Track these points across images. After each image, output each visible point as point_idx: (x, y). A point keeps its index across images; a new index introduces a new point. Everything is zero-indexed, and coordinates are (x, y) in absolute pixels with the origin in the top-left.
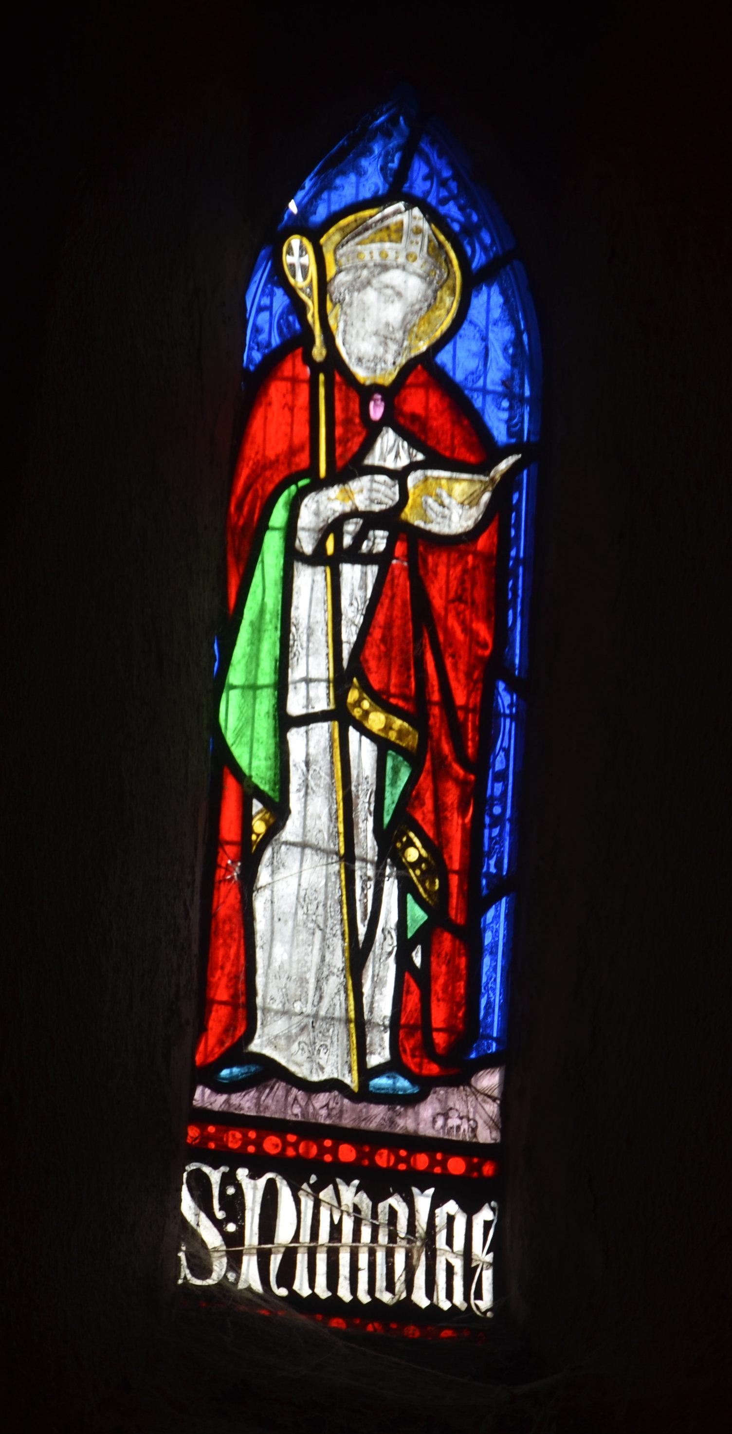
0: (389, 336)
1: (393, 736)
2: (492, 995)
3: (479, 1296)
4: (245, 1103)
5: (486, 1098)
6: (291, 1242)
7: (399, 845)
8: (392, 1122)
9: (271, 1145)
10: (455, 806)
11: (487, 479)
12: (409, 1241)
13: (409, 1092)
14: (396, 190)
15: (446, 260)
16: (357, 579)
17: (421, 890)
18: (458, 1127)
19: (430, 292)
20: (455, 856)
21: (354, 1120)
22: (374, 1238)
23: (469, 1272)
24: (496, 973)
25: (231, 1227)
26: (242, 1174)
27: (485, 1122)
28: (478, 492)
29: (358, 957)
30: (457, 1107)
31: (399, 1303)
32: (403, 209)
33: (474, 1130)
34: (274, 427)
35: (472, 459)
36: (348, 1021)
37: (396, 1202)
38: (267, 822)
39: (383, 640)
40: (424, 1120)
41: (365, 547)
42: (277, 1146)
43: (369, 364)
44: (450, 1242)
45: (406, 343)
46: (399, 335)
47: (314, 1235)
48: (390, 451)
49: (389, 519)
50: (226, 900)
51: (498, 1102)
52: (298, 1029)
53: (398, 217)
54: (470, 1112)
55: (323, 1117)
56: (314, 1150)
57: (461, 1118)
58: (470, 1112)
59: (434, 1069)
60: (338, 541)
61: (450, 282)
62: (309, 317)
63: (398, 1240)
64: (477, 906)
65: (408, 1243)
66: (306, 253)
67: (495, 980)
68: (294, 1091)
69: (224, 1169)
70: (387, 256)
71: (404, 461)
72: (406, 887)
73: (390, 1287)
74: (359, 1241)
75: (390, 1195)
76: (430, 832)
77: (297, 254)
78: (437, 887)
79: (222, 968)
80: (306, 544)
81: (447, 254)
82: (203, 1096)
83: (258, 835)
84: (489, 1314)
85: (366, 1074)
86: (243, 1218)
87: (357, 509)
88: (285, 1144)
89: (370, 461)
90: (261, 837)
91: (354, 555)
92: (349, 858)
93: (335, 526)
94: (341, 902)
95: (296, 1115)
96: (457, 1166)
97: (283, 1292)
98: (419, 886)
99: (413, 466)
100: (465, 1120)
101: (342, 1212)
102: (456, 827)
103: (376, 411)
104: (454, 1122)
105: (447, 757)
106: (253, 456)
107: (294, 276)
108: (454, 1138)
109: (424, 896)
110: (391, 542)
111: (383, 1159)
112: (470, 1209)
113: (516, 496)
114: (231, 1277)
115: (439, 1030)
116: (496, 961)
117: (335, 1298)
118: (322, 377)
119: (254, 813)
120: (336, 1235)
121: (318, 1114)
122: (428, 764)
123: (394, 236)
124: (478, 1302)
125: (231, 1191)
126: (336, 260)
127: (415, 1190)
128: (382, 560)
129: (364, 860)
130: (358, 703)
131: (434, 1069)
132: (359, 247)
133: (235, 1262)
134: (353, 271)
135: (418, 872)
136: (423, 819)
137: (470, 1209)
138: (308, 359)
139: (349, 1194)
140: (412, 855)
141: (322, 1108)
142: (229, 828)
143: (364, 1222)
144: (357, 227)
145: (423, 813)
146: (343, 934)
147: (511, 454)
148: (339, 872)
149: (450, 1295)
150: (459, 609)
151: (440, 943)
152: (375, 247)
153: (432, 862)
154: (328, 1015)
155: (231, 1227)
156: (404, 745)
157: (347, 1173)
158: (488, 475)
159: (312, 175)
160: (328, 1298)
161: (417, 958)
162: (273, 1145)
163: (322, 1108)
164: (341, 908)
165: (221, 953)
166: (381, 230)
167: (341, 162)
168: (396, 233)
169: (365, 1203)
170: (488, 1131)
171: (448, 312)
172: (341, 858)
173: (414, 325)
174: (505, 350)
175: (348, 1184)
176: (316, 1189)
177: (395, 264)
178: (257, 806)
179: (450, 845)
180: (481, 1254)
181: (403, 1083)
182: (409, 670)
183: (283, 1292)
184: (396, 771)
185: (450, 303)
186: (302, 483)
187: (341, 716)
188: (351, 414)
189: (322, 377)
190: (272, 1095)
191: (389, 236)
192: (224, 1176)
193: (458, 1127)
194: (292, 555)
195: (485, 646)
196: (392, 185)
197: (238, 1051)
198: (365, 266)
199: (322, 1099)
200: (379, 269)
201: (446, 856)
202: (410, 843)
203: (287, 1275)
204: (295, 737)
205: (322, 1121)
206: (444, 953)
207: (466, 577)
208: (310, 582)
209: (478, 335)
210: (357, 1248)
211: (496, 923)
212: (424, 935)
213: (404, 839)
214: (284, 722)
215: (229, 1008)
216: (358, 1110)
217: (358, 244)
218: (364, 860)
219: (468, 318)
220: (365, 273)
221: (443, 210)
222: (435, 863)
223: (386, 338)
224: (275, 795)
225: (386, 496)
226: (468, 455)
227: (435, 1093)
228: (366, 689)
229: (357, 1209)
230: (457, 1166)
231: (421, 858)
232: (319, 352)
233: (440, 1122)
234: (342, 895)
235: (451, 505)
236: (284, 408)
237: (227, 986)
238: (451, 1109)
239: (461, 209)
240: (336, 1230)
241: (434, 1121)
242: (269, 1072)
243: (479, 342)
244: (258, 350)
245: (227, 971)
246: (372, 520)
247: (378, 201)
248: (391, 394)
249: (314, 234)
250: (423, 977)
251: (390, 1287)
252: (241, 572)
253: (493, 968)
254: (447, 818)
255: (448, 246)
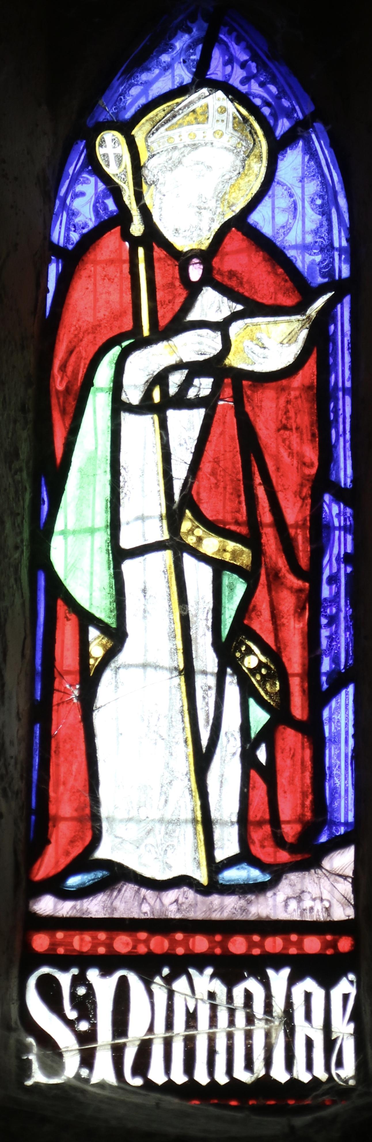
0: (203, 205)
1: (227, 557)
2: (337, 781)
3: (340, 1064)
4: (95, 907)
5: (337, 878)
6: (146, 1035)
7: (238, 655)
8: (244, 910)
9: (122, 944)
10: (292, 612)
11: (304, 317)
12: (267, 1021)
13: (260, 880)
14: (202, 79)
15: (250, 132)
16: (185, 424)
17: (262, 693)
18: (312, 908)
19: (239, 163)
20: (295, 660)
21: (205, 912)
22: (232, 1023)
23: (329, 1044)
24: (340, 760)
25: (84, 1026)
26: (93, 975)
27: (338, 901)
28: (296, 330)
29: (203, 760)
30: (310, 890)
31: (259, 1081)
32: (207, 94)
33: (327, 910)
34: (96, 298)
35: (289, 301)
36: (194, 821)
37: (252, 984)
38: (104, 646)
39: (214, 473)
40: (275, 906)
41: (192, 393)
42: (128, 944)
43: (185, 234)
44: (308, 1017)
45: (219, 210)
46: (212, 204)
47: (169, 1025)
48: (211, 305)
49: (214, 367)
50: (65, 721)
51: (350, 880)
52: (144, 833)
53: (203, 102)
54: (326, 892)
55: (173, 913)
56: (166, 944)
57: (314, 900)
58: (326, 892)
59: (284, 856)
60: (164, 392)
61: (256, 151)
62: (126, 199)
63: (256, 1021)
64: (319, 699)
65: (266, 1023)
66: (119, 145)
67: (340, 767)
68: (143, 891)
69: (75, 971)
70: (195, 136)
71: (226, 313)
72: (247, 691)
73: (249, 1066)
74: (216, 1027)
75: (243, 978)
76: (270, 640)
77: (111, 147)
78: (278, 688)
79: (64, 784)
80: (133, 394)
81: (251, 125)
82: (46, 905)
83: (96, 659)
84: (352, 1082)
85: (215, 868)
86: (95, 1016)
87: (181, 361)
88: (137, 942)
89: (193, 316)
90: (99, 660)
91: (181, 402)
92: (188, 672)
93: (160, 379)
94: (182, 712)
95: (146, 913)
96: (312, 945)
97: (138, 1082)
98: (260, 690)
99: (235, 316)
100: (318, 901)
101: (196, 999)
102: (294, 631)
103: (195, 273)
104: (307, 903)
105: (281, 569)
106: (74, 323)
107: (108, 165)
108: (308, 919)
109: (266, 698)
110: (216, 387)
111: (238, 945)
112: (327, 983)
113: (332, 327)
114: (84, 1072)
115: (288, 822)
116: (340, 749)
117: (192, 1083)
118: (141, 251)
119: (90, 639)
120: (192, 1024)
121: (167, 910)
122: (263, 578)
123: (201, 118)
124: (340, 1072)
125: (82, 991)
126: (148, 147)
127: (270, 972)
128: (208, 403)
129: (204, 673)
130: (191, 531)
131: (284, 856)
132: (169, 133)
133: (88, 1060)
134: (165, 153)
135: (258, 677)
136: (261, 629)
137: (327, 983)
138: (126, 235)
139: (205, 981)
140: (250, 662)
141: (172, 904)
142: (67, 656)
143: (219, 1008)
144: (166, 115)
145: (261, 623)
146: (186, 741)
147: (325, 293)
148: (179, 685)
149: (309, 1066)
150: (285, 437)
151: (283, 739)
152: (185, 130)
153: (272, 667)
154: (174, 818)
155: (84, 1026)
156: (238, 564)
157: (200, 962)
158: (304, 314)
159: (119, 75)
160: (185, 1083)
161: (262, 754)
162: (123, 943)
163: (172, 904)
164: (183, 717)
165: (63, 769)
166: (188, 115)
167: (140, 57)
168: (201, 117)
169: (219, 988)
170: (342, 908)
171: (257, 176)
172: (180, 673)
173: (225, 193)
174: (313, 201)
175: (201, 971)
176: (169, 980)
177: (203, 142)
178: (93, 633)
179: (288, 649)
180: (343, 1029)
181: (255, 874)
182: (239, 496)
183: (138, 1082)
184: (232, 588)
185: (258, 169)
186: (125, 344)
187: (177, 545)
188: (171, 282)
189: (141, 251)
190: (120, 896)
191: (196, 119)
192: (75, 978)
193: (312, 908)
194: (119, 406)
195: (312, 465)
196: (196, 75)
197: (84, 862)
198: (175, 148)
199: (170, 896)
200: (189, 149)
201: (284, 659)
202: (249, 651)
203: (142, 1065)
204: (128, 566)
205: (173, 917)
206: (287, 748)
207: (289, 406)
208: (140, 429)
209: (286, 193)
210: (214, 1034)
211: (341, 715)
212: (268, 734)
213: (243, 648)
214: (119, 555)
215: (75, 823)
216: (209, 902)
217: (166, 130)
218: (204, 673)
219: (276, 180)
220: (176, 154)
221: (244, 89)
222: (277, 669)
223: (200, 208)
224: (111, 621)
225: (209, 347)
226: (284, 299)
227: (286, 878)
228: (200, 518)
229: (212, 995)
230: (312, 945)
231: (261, 664)
232: (137, 228)
233: (293, 904)
234: (182, 706)
235: (270, 344)
236: (104, 279)
237: (70, 800)
238: (303, 892)
239: (262, 85)
240: (191, 1018)
241: (286, 905)
242: (117, 875)
243: (288, 198)
244: (75, 231)
245: (69, 786)
246: (196, 369)
247: (182, 91)
248: (206, 256)
249: (126, 128)
250: (269, 773)
251: (249, 1066)
252: (67, 425)
253: (340, 756)
254: (284, 625)
255: (252, 119)
